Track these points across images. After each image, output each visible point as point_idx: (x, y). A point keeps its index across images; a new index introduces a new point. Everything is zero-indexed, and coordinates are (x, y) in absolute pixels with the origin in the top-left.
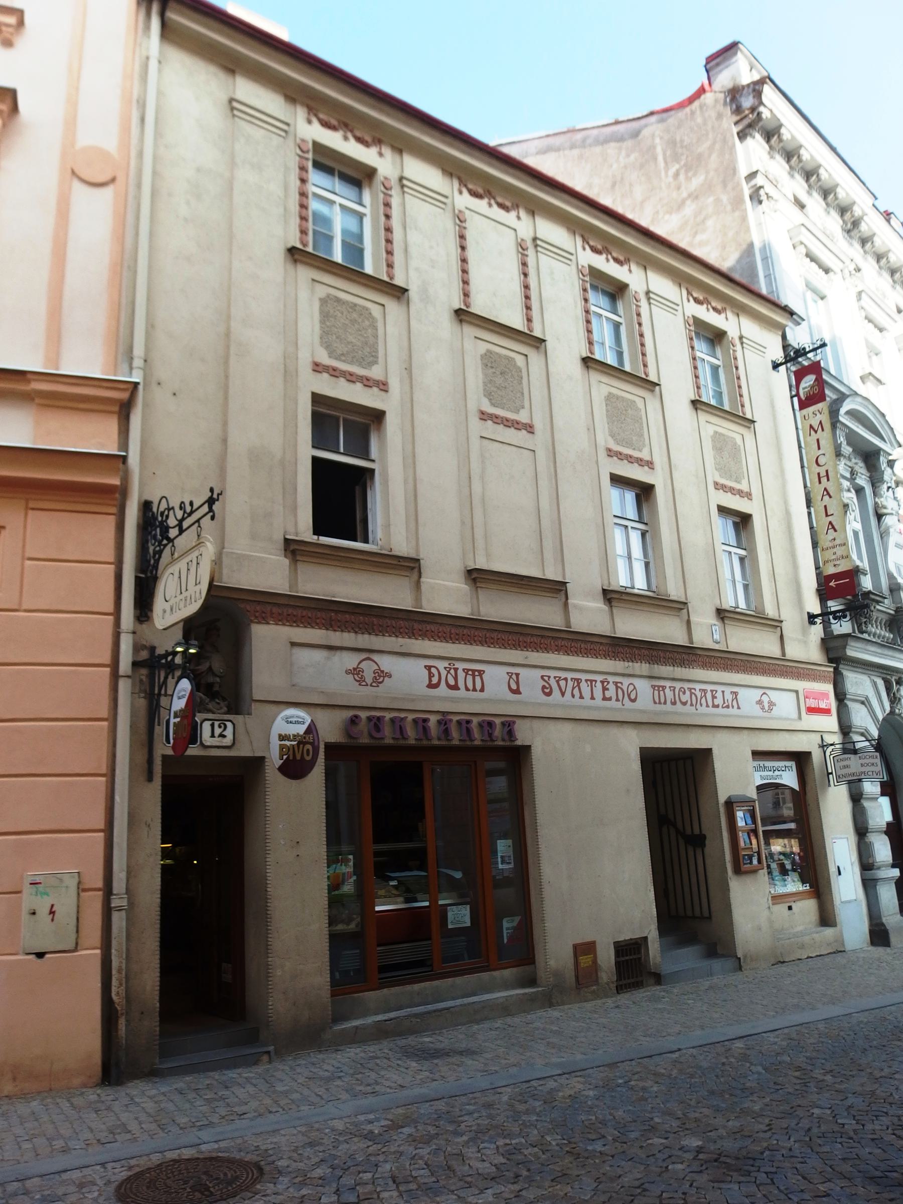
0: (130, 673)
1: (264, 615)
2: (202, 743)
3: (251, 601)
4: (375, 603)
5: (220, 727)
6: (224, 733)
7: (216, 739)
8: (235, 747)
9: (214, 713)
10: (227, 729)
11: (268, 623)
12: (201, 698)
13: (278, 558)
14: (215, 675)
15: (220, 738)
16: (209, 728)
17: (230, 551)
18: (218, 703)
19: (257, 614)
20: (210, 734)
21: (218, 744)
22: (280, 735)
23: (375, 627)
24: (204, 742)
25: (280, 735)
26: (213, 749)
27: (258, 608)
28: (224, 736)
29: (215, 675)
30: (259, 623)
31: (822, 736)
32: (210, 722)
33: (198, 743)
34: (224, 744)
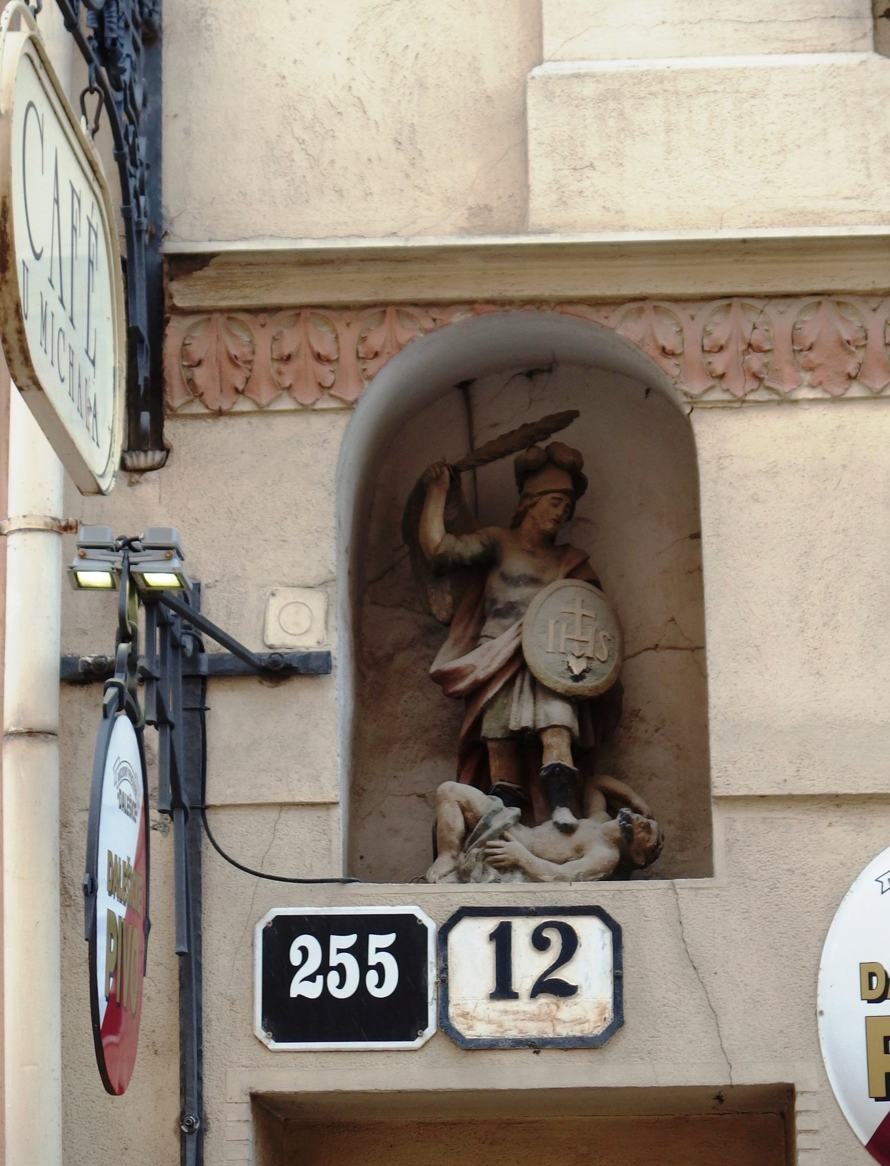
0: (47, 717)
1: (755, 361)
2: (445, 1026)
3: (344, 307)
4: (818, 223)
5: (540, 943)
6: (566, 974)
7: (524, 1005)
8: (626, 1038)
9: (532, 877)
10: (580, 954)
11: (787, 401)
12: (465, 808)
13: (825, 59)
14: (539, 689)
15: (544, 1000)
16: (487, 953)
17: (568, 68)
18: (567, 830)
19: (719, 363)
20: (488, 982)
21: (533, 1030)
22: (869, 973)
23: (201, 376)
24: (459, 1025)
25: (869, 973)
26: (507, 1058)
27: (721, 331)
28: (565, 990)
29: (539, 689)
30: (739, 403)
31: (335, 804)
32: (491, 924)
33: (431, 1028)
34: (564, 1031)
